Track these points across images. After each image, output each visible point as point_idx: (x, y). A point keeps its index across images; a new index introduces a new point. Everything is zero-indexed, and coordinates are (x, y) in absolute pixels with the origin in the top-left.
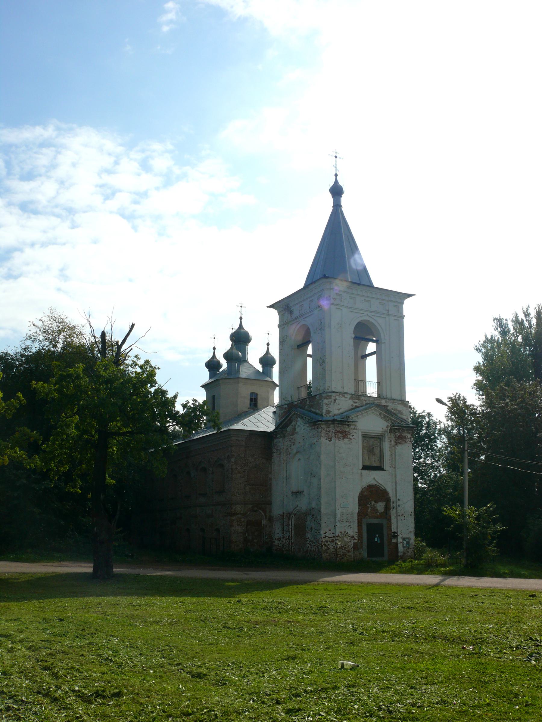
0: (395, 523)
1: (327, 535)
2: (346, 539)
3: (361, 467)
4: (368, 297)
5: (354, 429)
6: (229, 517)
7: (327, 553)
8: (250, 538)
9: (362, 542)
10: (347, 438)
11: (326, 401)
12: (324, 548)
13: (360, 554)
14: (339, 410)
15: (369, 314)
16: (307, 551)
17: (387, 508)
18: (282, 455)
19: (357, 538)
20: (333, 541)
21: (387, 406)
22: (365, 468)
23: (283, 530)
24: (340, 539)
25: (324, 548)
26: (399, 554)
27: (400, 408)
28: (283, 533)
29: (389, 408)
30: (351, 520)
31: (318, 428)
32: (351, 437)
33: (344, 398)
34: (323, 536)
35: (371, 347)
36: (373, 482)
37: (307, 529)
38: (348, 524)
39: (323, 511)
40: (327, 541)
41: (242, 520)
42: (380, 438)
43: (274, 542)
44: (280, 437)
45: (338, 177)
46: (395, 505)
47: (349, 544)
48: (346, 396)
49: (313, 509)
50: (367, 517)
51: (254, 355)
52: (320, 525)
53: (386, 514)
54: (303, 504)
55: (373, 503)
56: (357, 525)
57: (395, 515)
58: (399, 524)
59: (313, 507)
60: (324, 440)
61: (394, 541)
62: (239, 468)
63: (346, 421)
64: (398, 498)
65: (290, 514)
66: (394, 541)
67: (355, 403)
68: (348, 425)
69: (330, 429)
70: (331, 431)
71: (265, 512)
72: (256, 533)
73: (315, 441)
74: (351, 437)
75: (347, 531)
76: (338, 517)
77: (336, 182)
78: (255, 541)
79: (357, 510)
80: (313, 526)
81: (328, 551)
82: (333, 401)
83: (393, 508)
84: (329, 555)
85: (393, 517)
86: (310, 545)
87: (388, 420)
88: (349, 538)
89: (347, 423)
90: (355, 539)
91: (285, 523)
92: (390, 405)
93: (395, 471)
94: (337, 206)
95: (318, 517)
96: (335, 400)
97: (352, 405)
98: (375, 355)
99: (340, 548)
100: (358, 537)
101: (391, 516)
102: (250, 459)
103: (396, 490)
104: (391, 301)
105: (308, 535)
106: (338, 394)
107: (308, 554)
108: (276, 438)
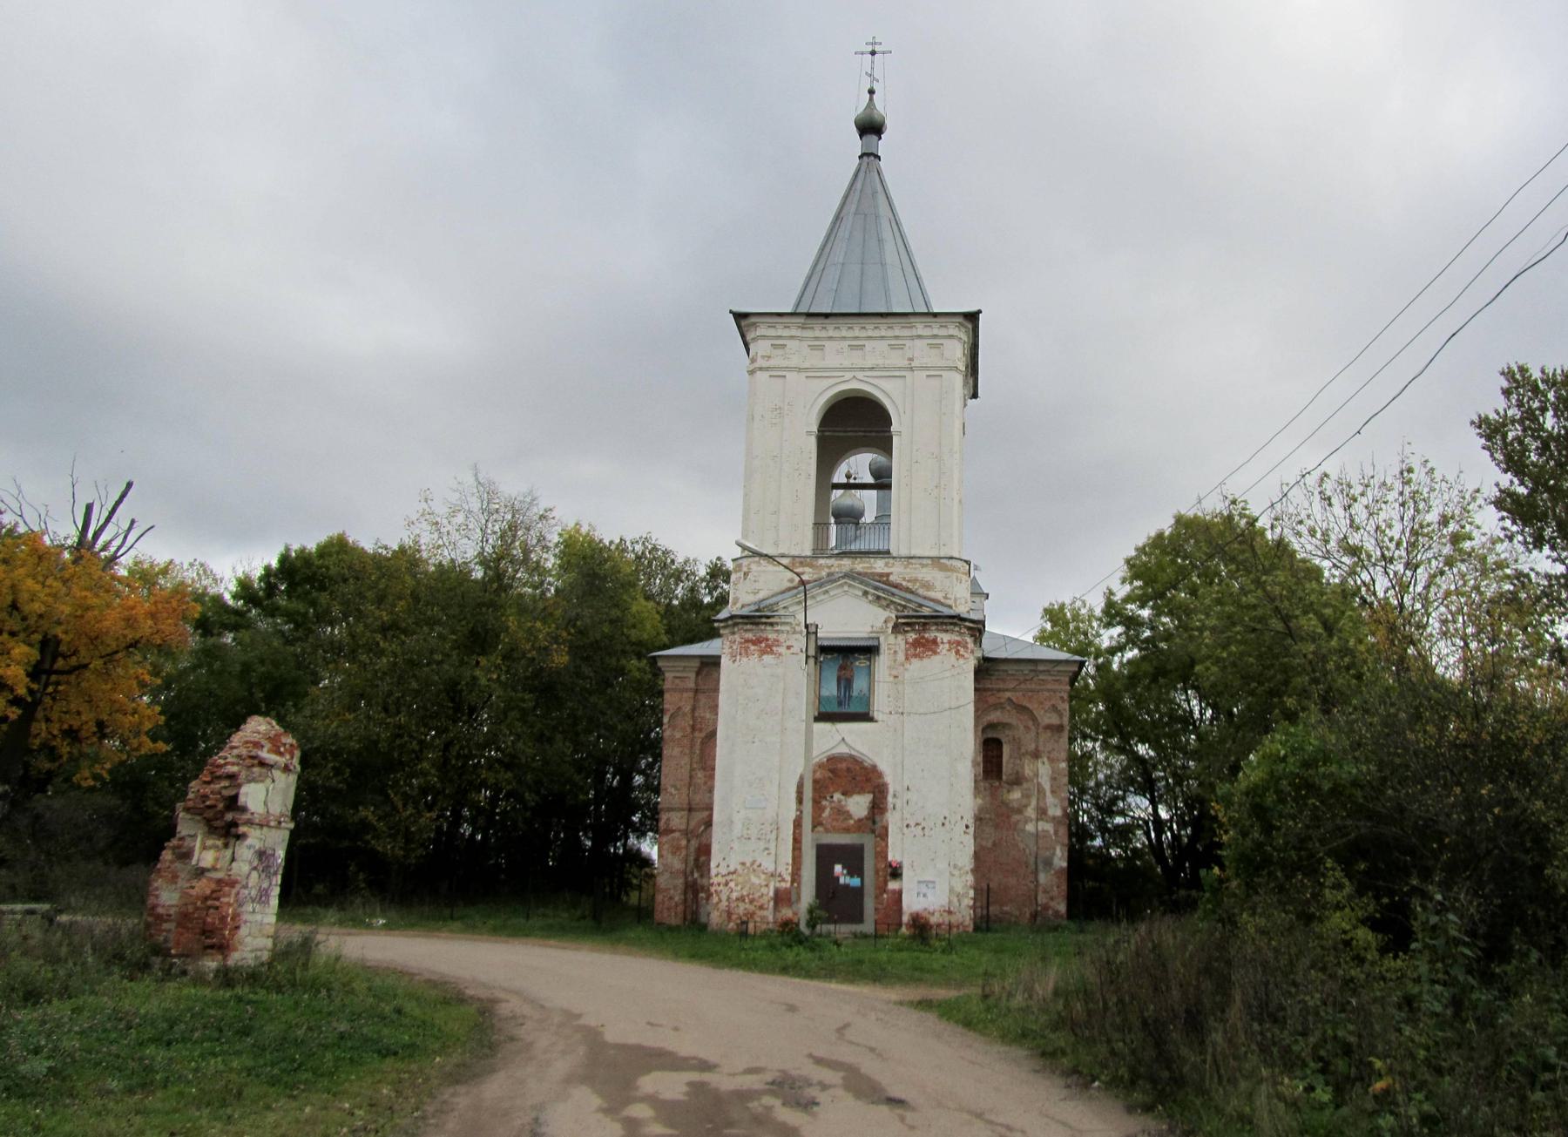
2: (754, 880)
10: (772, 652)
15: (860, 375)
17: (878, 807)
19: (789, 878)
22: (823, 717)
29: (892, 578)
38: (762, 845)
47: (764, 890)
55: (837, 796)
61: (893, 885)
68: (772, 624)
74: (782, 650)
101: (886, 829)
104: (919, 337)
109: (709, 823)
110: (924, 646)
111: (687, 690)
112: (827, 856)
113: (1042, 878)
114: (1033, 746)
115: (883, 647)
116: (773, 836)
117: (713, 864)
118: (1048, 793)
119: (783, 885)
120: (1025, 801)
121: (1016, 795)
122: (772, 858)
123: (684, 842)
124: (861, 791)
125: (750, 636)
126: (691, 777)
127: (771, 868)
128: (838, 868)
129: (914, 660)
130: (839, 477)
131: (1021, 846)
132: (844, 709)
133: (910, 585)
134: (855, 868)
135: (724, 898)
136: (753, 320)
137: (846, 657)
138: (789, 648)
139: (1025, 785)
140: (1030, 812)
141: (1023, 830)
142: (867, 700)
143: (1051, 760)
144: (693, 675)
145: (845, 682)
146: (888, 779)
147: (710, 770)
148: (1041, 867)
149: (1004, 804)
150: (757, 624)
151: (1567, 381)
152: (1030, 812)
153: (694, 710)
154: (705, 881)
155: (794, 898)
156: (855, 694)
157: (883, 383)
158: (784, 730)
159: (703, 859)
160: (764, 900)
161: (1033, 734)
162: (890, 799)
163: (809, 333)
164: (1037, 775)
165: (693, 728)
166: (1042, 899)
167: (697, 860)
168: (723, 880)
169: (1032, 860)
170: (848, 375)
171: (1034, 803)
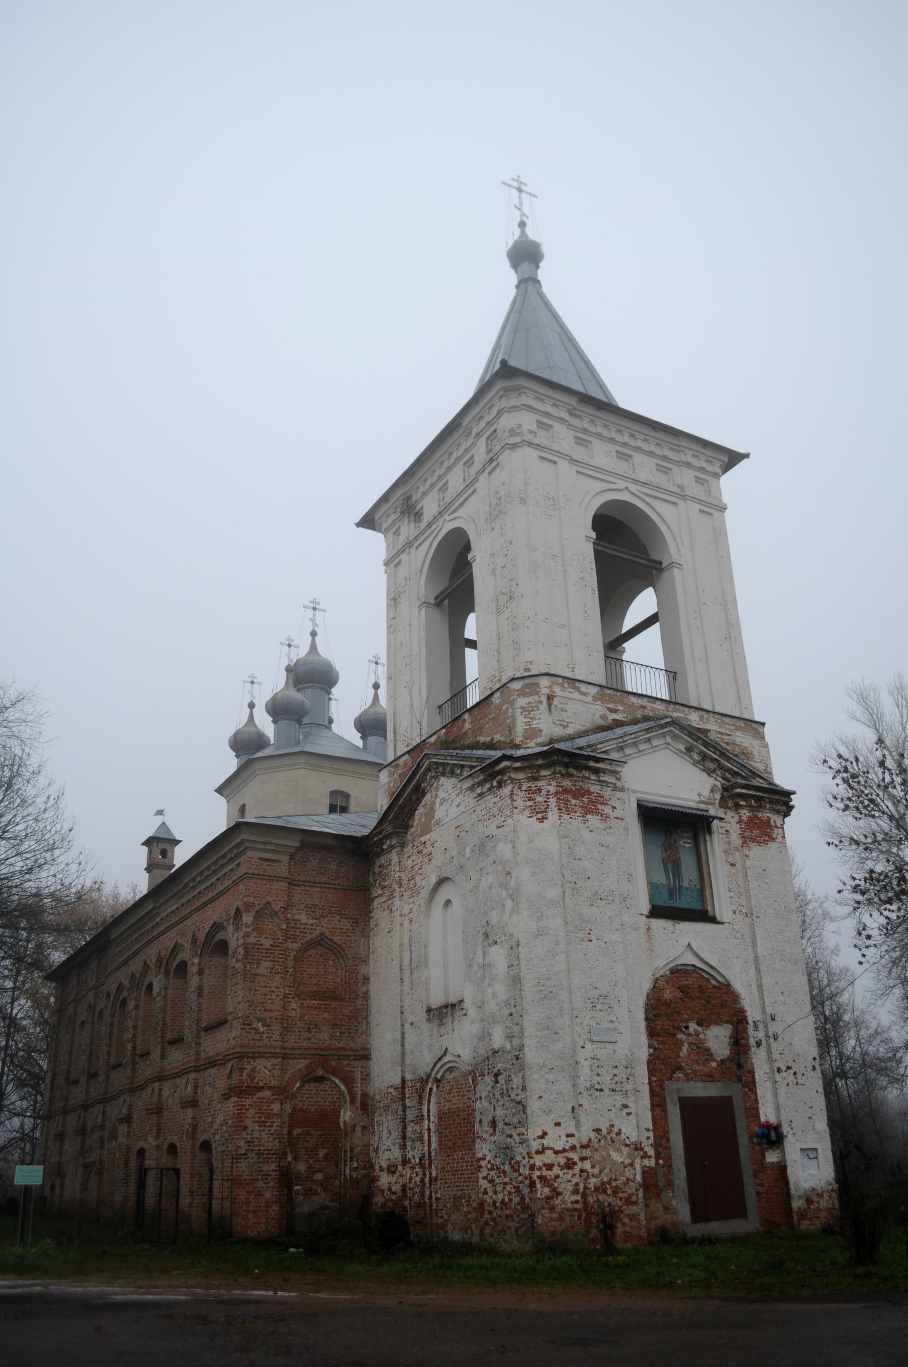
0: (769, 1096)
1: (546, 1142)
2: (616, 1157)
3: (645, 908)
4: (625, 444)
5: (615, 788)
6: (234, 1099)
7: (552, 1209)
8: (302, 1167)
9: (668, 1159)
10: (596, 812)
11: (523, 701)
12: (542, 1191)
13: (666, 1208)
14: (565, 727)
15: (633, 488)
16: (482, 1204)
17: (739, 1043)
18: (397, 901)
19: (651, 1152)
20: (569, 1165)
21: (706, 732)
22: (657, 912)
23: (404, 1137)
25: (542, 1191)
27: (743, 739)
28: (403, 1147)
29: (712, 736)
30: (629, 1087)
31: (500, 785)
32: (607, 810)
33: (576, 695)
34: (535, 1145)
35: (645, 603)
36: (689, 959)
37: (477, 1127)
38: (619, 1100)
39: (531, 1056)
40: (549, 1167)
41: (276, 1107)
43: (377, 1178)
44: (392, 847)
46: (761, 1035)
47: (628, 1172)
48: (583, 688)
49: (495, 1052)
50: (679, 1075)
51: (346, 707)
52: (521, 1106)
54: (462, 1042)
55: (693, 1027)
56: (648, 1104)
57: (766, 1068)
58: (781, 1099)
59: (496, 1046)
60: (526, 822)
61: (772, 1157)
62: (267, 944)
63: (589, 758)
64: (769, 1010)
65: (424, 1081)
68: (596, 771)
69: (540, 784)
70: (545, 788)
71: (348, 1081)
72: (322, 1153)
73: (492, 829)
75: (617, 1126)
76: (585, 1076)
77: (530, 309)
78: (319, 1176)
79: (643, 1053)
80: (500, 1112)
81: (557, 1202)
82: (544, 699)
83: (759, 1044)
84: (561, 1219)
85: (760, 1076)
86: (491, 1181)
87: (714, 771)
88: (625, 1150)
89: (592, 764)
90: (646, 1156)
91: (411, 1114)
92: (712, 725)
93: (752, 926)
95: (516, 1082)
96: (550, 698)
97: (603, 717)
98: (656, 627)
99: (597, 1189)
100: (655, 1146)
101: (752, 1073)
102: (304, 918)
103: (760, 986)
104: (688, 465)
105: (484, 1149)
107: (486, 1216)
108: (379, 855)
110: (758, 827)
111: (279, 878)
124: (719, 1022)
125: (567, 783)
129: (753, 846)
136: (522, 381)
144: (285, 859)
150: (579, 768)
157: (657, 505)
160: (630, 1189)
163: (575, 422)
170: (621, 484)
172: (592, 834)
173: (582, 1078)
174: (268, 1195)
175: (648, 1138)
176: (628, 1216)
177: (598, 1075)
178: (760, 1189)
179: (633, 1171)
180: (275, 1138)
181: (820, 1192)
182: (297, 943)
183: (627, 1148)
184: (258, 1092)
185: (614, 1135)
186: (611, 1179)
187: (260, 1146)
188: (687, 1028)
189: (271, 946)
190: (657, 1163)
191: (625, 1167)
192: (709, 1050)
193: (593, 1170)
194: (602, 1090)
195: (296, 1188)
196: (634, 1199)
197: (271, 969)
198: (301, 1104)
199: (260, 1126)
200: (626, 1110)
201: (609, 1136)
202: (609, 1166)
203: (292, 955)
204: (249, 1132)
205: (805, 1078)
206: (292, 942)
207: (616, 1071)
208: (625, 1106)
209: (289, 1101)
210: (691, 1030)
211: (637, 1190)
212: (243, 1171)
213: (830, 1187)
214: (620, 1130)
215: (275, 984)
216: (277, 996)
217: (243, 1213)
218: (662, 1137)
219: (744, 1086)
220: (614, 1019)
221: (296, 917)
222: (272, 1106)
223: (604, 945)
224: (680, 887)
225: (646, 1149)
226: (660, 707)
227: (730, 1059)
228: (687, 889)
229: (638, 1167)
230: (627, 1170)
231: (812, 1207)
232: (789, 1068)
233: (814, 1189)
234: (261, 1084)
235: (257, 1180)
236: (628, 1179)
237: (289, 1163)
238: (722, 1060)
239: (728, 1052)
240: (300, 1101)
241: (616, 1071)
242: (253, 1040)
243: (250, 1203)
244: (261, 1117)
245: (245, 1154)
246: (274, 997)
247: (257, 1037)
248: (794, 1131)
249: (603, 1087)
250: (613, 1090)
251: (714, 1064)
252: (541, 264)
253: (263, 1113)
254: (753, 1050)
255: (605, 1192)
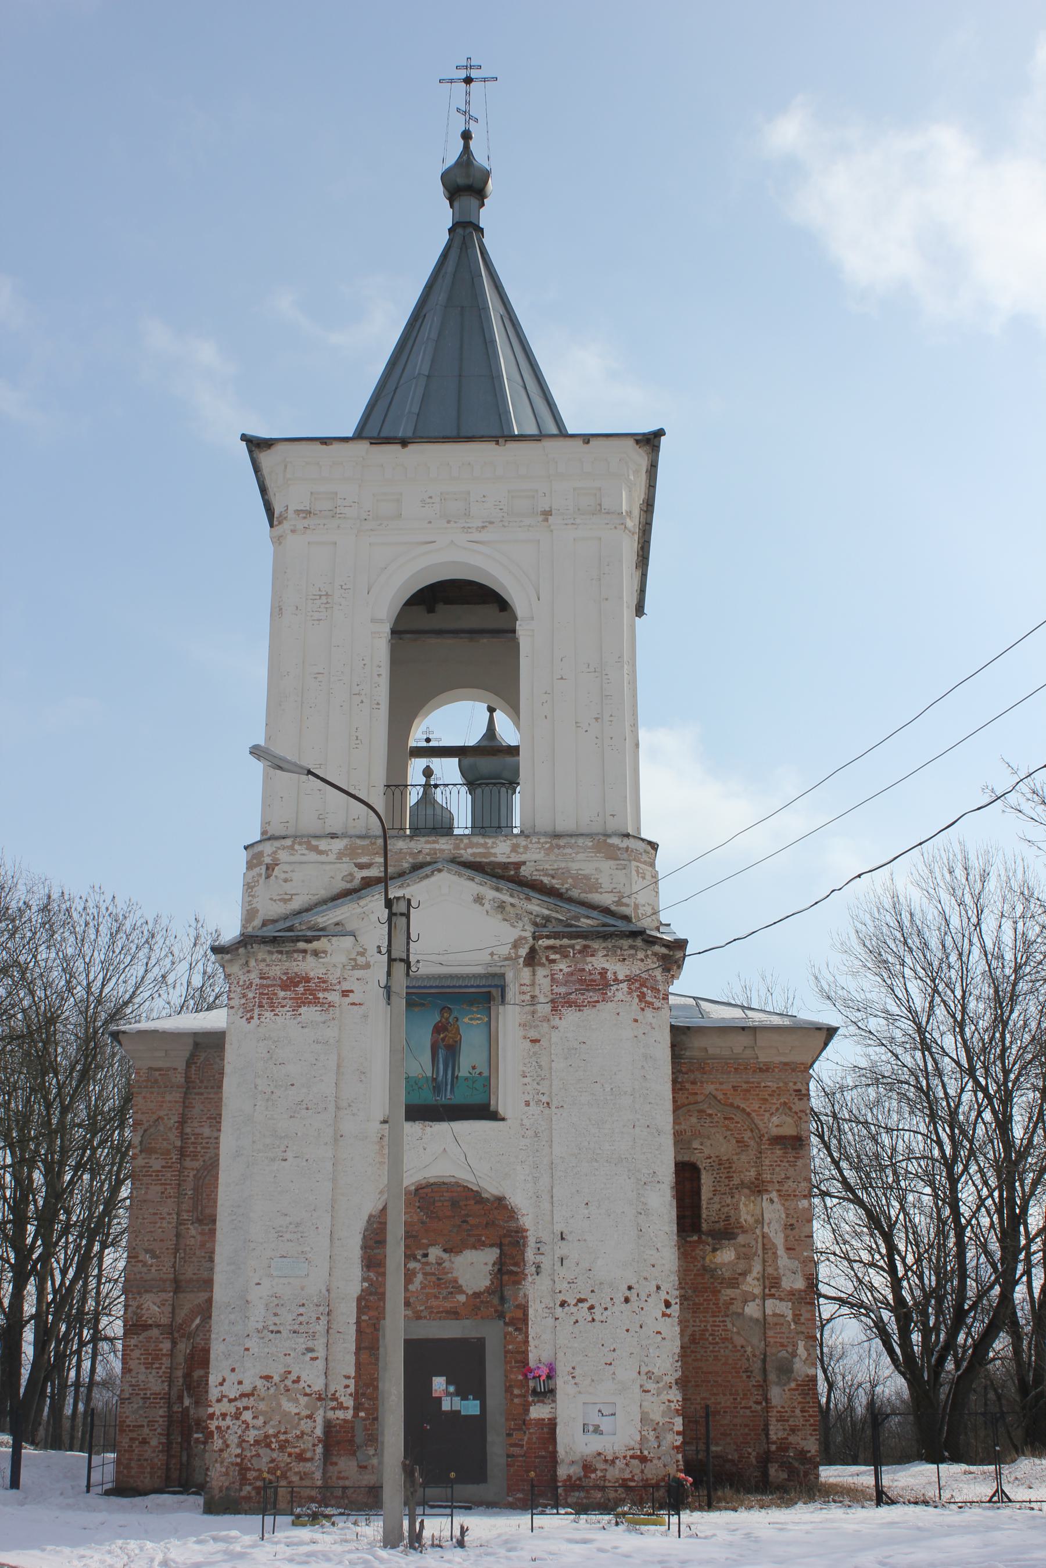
9: (374, 1418)
10: (316, 1001)
17: (509, 1270)
19: (349, 1402)
24: (262, 1406)
26: (562, 1472)
29: (524, 871)
33: (313, 856)
38: (301, 1342)
42: (484, 994)
45: (472, 143)
47: (306, 1425)
48: (323, 844)
53: (502, 1299)
55: (435, 1253)
61: (538, 1412)
66: (538, 1412)
67: (361, 866)
74: (334, 997)
88: (303, 1400)
90: (341, 1407)
94: (465, 233)
99: (257, 1442)
100: (356, 1396)
101: (524, 1308)
106: (288, 842)
109: (206, 1310)
112: (422, 1359)
113: (777, 1395)
114: (753, 1173)
115: (512, 993)
116: (320, 1328)
117: (213, 1379)
118: (781, 1251)
119: (340, 1414)
120: (741, 1266)
121: (726, 1256)
122: (320, 1364)
123: (166, 1346)
126: (178, 1235)
127: (318, 1385)
128: (439, 1383)
130: (416, 738)
131: (739, 1341)
132: (449, 1097)
133: (556, 883)
134: (471, 1383)
135: (233, 1440)
137: (447, 1006)
138: (345, 993)
139: (741, 1239)
140: (752, 1284)
141: (740, 1315)
142: (486, 1082)
143: (784, 1197)
145: (446, 1046)
146: (527, 1221)
147: (208, 1221)
148: (772, 1377)
149: (708, 1271)
151: (1045, 908)
152: (752, 1284)
153: (182, 1122)
154: (202, 1413)
155: (360, 1437)
156: (464, 1071)
158: (338, 1137)
159: (198, 1373)
160: (307, 1443)
161: (752, 1153)
162: (530, 1255)
164: (760, 1221)
165: (182, 1153)
166: (776, 1432)
167: (187, 1376)
168: (231, 1409)
169: (757, 1365)
171: (757, 1268)
172: (306, 1030)
173: (252, 1318)
174: (154, 1442)
175: (347, 1387)
176: (296, 1473)
177: (276, 1314)
178: (516, 1450)
179: (313, 1424)
180: (163, 1382)
181: (609, 1458)
182: (198, 1160)
183: (306, 1398)
184: (144, 1331)
185: (288, 1382)
186: (279, 1432)
187: (146, 1389)
188: (426, 1255)
189: (163, 1167)
190: (356, 1415)
191: (300, 1419)
192: (456, 1281)
193: (255, 1421)
194: (278, 1332)
195: (196, 1436)
196: (309, 1455)
197: (162, 1193)
198: (203, 1342)
199: (147, 1368)
200: (310, 1355)
201: (288, 1384)
202: (278, 1418)
203: (191, 1175)
204: (134, 1374)
205: (606, 1313)
206: (192, 1160)
207: (302, 1310)
208: (310, 1350)
209: (184, 1340)
210: (432, 1258)
211: (314, 1445)
212: (127, 1417)
213: (631, 1452)
214: (299, 1377)
215: (166, 1210)
216: (169, 1223)
217: (125, 1462)
218: (367, 1386)
219: (506, 1324)
220: (308, 1249)
221: (197, 1131)
222: (161, 1346)
223: (305, 1163)
224: (455, 1078)
225: (342, 1399)
226: (444, 847)
227: (488, 1291)
228: (466, 1079)
229: (320, 1420)
230: (302, 1422)
231: (593, 1476)
232: (581, 1300)
233: (599, 1454)
234: (150, 1322)
235: (143, 1426)
236: (303, 1433)
237: (187, 1408)
238: (475, 1293)
239: (488, 1283)
240: (202, 1339)
241: (302, 1310)
242: (140, 1273)
243: (133, 1451)
244: (147, 1359)
245: (129, 1399)
246: (165, 1225)
247: (145, 1269)
248: (576, 1381)
249: (281, 1329)
250: (295, 1332)
251: (462, 1298)
252: (485, 201)
253: (150, 1354)
254: (530, 1279)
255: (268, 1446)
